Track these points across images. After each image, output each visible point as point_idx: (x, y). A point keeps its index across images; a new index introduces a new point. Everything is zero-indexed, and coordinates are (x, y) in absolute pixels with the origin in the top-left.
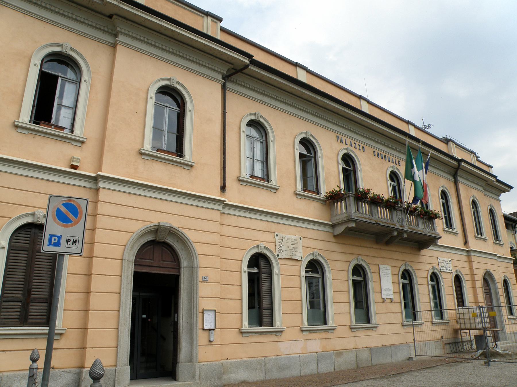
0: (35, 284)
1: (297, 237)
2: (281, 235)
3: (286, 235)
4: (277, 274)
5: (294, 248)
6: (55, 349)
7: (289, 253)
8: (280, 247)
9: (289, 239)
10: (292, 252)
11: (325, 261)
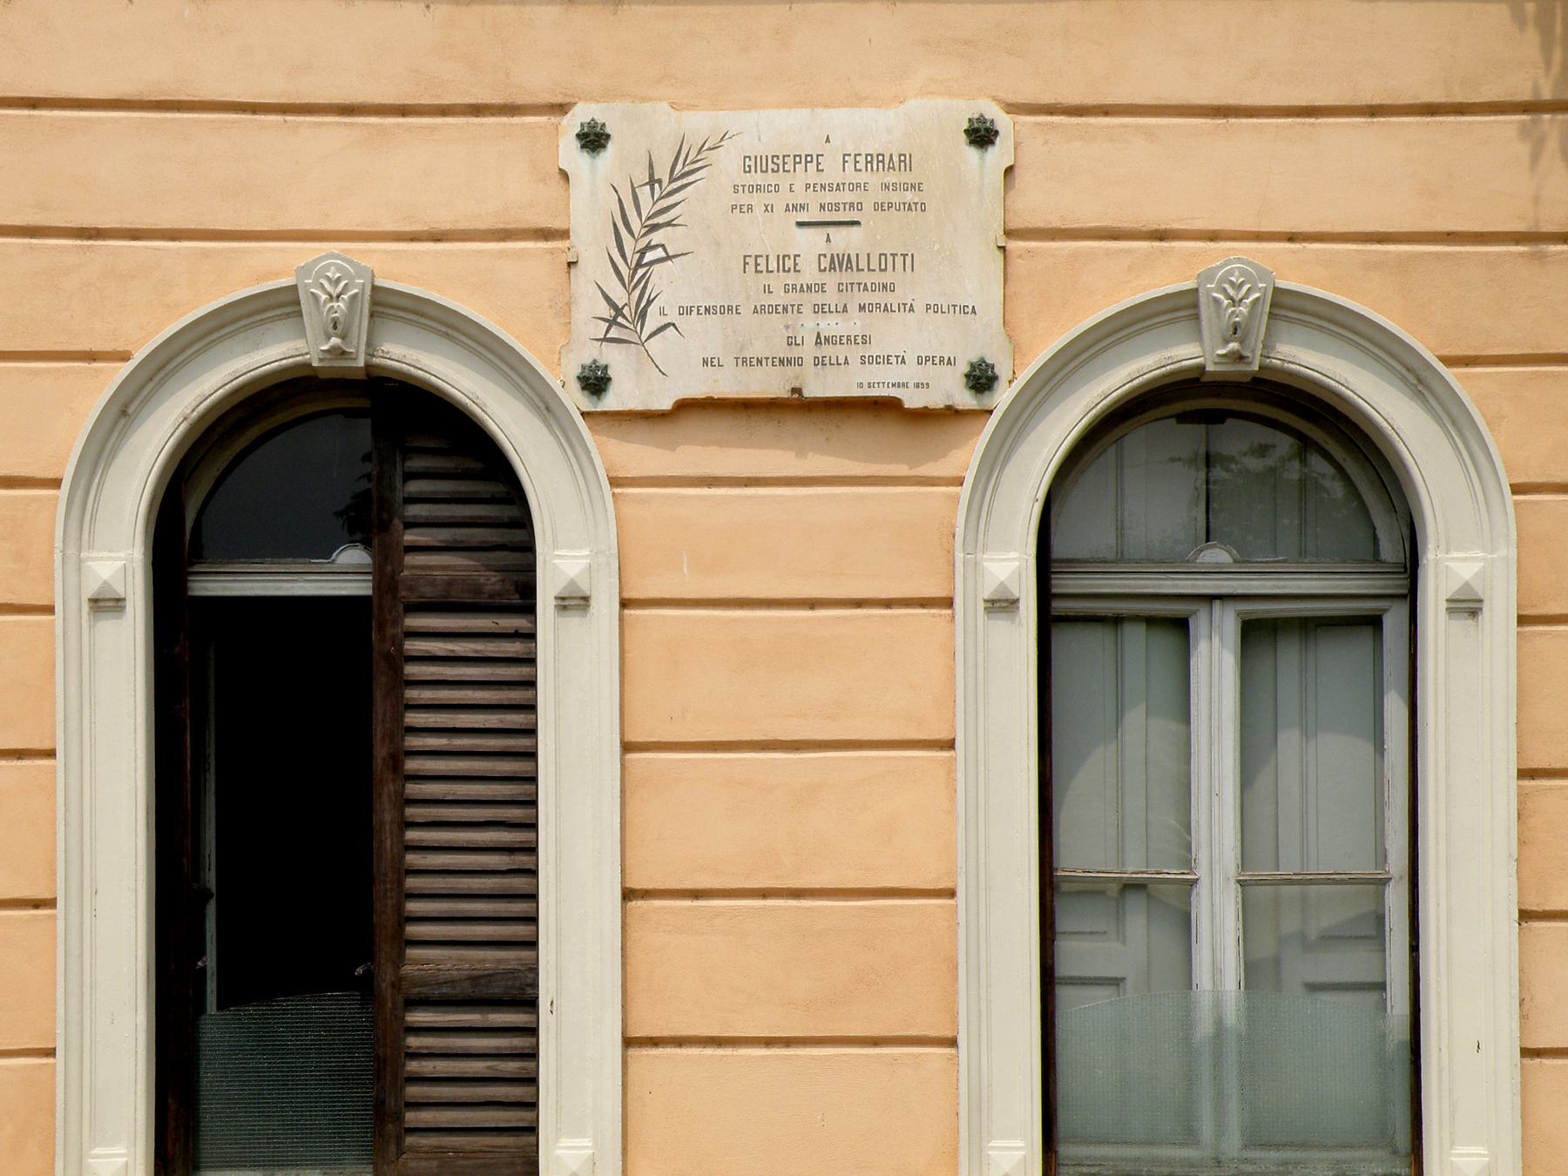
0: (427, 695)
1: (926, 116)
2: (646, 129)
3: (728, 120)
4: (574, 602)
5: (839, 263)
6: (1070, 893)
7: (767, 337)
8: (637, 270)
9: (777, 163)
10: (809, 325)
11: (1417, 378)
